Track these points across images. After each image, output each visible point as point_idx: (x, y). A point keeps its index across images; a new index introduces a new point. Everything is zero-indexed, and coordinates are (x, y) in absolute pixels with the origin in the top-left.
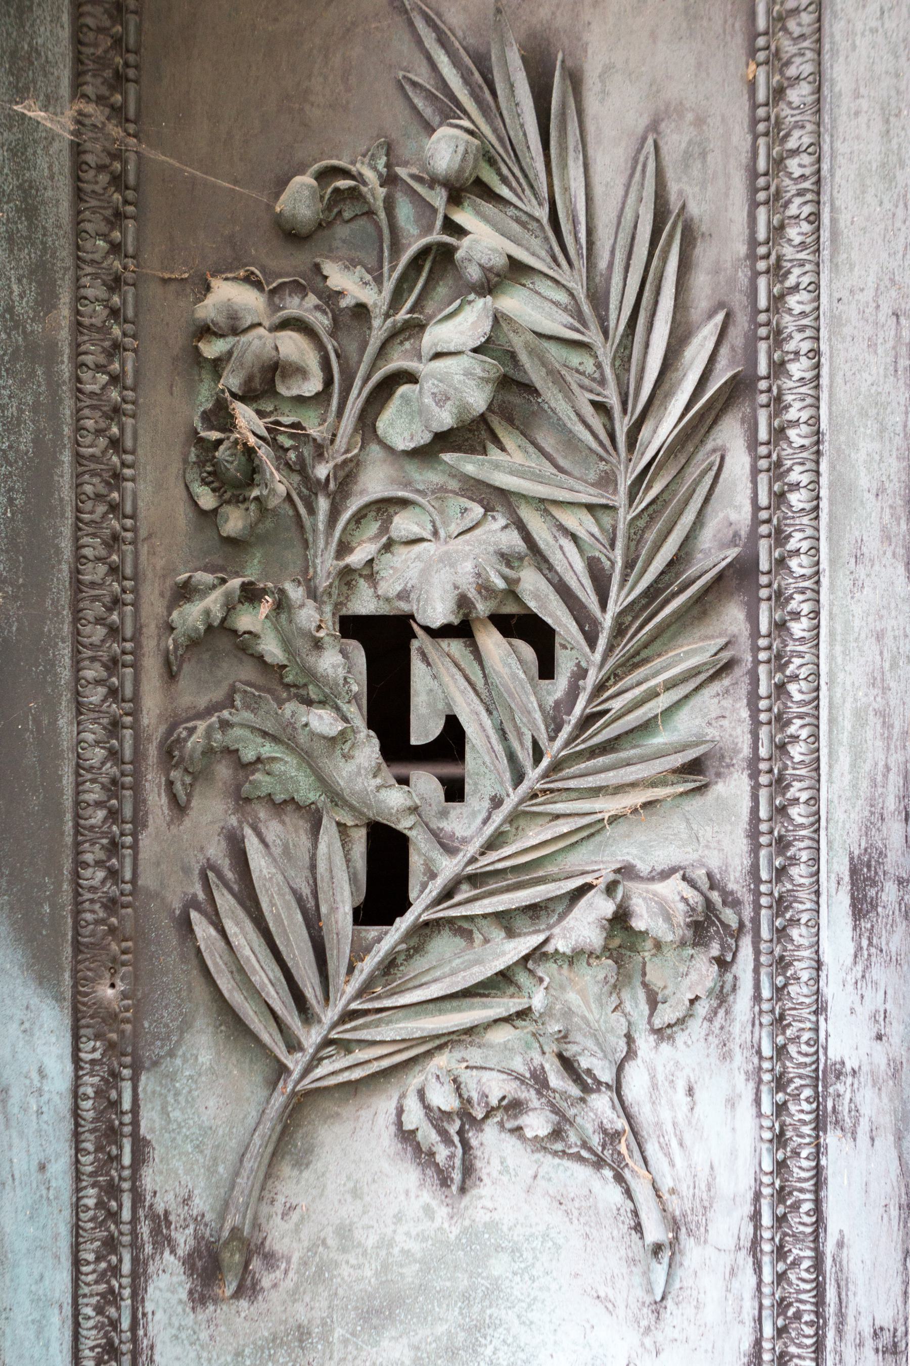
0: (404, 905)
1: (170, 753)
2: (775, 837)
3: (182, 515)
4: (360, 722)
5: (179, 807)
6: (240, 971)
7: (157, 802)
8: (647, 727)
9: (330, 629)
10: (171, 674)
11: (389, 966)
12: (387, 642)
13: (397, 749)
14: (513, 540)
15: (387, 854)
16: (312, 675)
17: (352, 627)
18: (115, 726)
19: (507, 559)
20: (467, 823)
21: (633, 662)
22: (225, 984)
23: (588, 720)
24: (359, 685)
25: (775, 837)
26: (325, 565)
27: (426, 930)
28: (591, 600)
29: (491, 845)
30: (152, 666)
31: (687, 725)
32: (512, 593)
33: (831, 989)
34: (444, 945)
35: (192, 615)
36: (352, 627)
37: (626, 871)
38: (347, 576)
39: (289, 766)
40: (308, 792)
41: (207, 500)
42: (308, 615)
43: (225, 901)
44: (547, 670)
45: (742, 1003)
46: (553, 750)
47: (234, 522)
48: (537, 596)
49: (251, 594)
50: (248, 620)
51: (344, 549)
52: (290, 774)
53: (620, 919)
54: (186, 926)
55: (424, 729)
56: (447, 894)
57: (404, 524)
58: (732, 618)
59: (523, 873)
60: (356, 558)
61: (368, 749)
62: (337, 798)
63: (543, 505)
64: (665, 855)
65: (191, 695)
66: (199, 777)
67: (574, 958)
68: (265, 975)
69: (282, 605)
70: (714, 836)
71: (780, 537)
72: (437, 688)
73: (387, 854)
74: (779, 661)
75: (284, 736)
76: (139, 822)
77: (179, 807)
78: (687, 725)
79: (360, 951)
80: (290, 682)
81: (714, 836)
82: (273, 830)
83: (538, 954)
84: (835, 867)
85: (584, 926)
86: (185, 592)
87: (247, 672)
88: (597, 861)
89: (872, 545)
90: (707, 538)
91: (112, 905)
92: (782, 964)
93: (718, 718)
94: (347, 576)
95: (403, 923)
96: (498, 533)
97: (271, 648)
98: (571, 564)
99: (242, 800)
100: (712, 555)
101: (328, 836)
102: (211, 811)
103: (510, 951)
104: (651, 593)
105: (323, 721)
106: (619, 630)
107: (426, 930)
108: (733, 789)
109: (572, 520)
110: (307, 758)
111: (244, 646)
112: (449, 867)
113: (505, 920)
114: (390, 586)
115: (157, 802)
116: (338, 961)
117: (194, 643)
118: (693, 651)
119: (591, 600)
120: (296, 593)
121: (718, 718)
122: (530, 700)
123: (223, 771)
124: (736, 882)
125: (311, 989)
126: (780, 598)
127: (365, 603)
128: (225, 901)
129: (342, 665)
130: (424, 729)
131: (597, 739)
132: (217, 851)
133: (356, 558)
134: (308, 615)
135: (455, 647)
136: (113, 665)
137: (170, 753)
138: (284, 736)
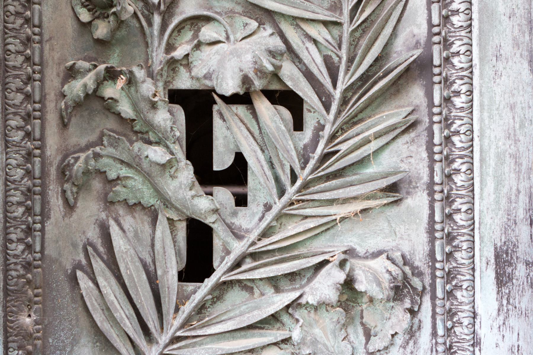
0: (209, 271)
1: (64, 172)
2: (445, 232)
3: (70, 26)
4: (180, 154)
5: (70, 207)
6: (107, 309)
7: (56, 203)
8: (362, 162)
9: (162, 96)
10: (64, 125)
11: (201, 309)
12: (198, 106)
13: (207, 177)
14: (277, 43)
15: (198, 260)
16: (150, 125)
17: (176, 97)
18: (29, 156)
19: (272, 54)
20: (249, 219)
21: (353, 121)
22: (99, 317)
23: (326, 157)
24: (180, 130)
25: (445, 232)
26: (159, 57)
27: (223, 287)
28: (327, 82)
29: (265, 234)
30: (52, 119)
31: (387, 162)
32: (275, 76)
33: (483, 331)
34: (235, 296)
35: (77, 88)
36: (176, 97)
37: (350, 252)
38: (172, 64)
39: (137, 182)
40: (149, 198)
41: (85, 16)
42: (147, 88)
43: (98, 265)
44: (298, 125)
45: (425, 337)
46: (303, 176)
47: (102, 30)
48: (292, 78)
49: (112, 75)
50: (110, 91)
51: (170, 48)
52: (137, 187)
53: (349, 284)
54: (74, 280)
55: (222, 161)
56: (238, 264)
57: (208, 32)
58: (416, 94)
59: (285, 252)
60: (179, 53)
61: (186, 172)
62: (167, 203)
63: (295, 20)
64: (374, 243)
65: (77, 136)
66: (81, 188)
67: (322, 306)
68: (123, 312)
69: (131, 81)
70: (406, 231)
71: (446, 44)
72: (230, 134)
73: (198, 260)
74: (447, 122)
75: (134, 164)
76: (45, 215)
77: (70, 207)
78: (387, 162)
79: (182, 299)
80: (136, 130)
81: (406, 231)
82: (128, 221)
83: (295, 304)
84: (484, 253)
85: (324, 287)
86: (72, 73)
87: (111, 123)
88: (333, 246)
89: (507, 49)
90: (399, 44)
91: (28, 266)
92: (451, 314)
93: (407, 157)
94: (172, 64)
95: (210, 282)
96: (267, 38)
97: (126, 109)
98: (314, 59)
99: (109, 203)
100: (403, 54)
101: (162, 226)
102: (89, 209)
103: (279, 301)
104: (364, 78)
105: (157, 154)
106: (344, 101)
107: (223, 287)
108: (418, 202)
109: (313, 31)
110: (148, 177)
111: (108, 107)
112: (238, 248)
113: (274, 282)
114: (199, 70)
115: (56, 203)
116: (169, 302)
117: (78, 105)
118: (392, 115)
119: (327, 82)
120: (140, 74)
121: (407, 157)
122: (291, 146)
123: (97, 185)
124: (420, 260)
125: (152, 323)
126: (447, 82)
127: (184, 82)
128: (98, 265)
129: (170, 120)
130: (222, 161)
131: (331, 168)
132: (93, 234)
133: (179, 53)
134: (147, 88)
135: (241, 110)
136: (28, 118)
137: (64, 172)
138: (134, 164)
